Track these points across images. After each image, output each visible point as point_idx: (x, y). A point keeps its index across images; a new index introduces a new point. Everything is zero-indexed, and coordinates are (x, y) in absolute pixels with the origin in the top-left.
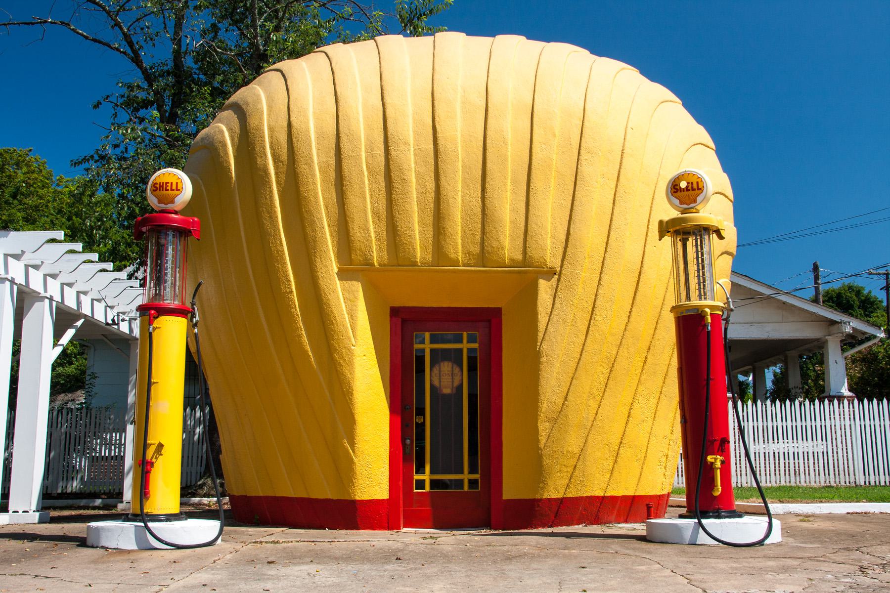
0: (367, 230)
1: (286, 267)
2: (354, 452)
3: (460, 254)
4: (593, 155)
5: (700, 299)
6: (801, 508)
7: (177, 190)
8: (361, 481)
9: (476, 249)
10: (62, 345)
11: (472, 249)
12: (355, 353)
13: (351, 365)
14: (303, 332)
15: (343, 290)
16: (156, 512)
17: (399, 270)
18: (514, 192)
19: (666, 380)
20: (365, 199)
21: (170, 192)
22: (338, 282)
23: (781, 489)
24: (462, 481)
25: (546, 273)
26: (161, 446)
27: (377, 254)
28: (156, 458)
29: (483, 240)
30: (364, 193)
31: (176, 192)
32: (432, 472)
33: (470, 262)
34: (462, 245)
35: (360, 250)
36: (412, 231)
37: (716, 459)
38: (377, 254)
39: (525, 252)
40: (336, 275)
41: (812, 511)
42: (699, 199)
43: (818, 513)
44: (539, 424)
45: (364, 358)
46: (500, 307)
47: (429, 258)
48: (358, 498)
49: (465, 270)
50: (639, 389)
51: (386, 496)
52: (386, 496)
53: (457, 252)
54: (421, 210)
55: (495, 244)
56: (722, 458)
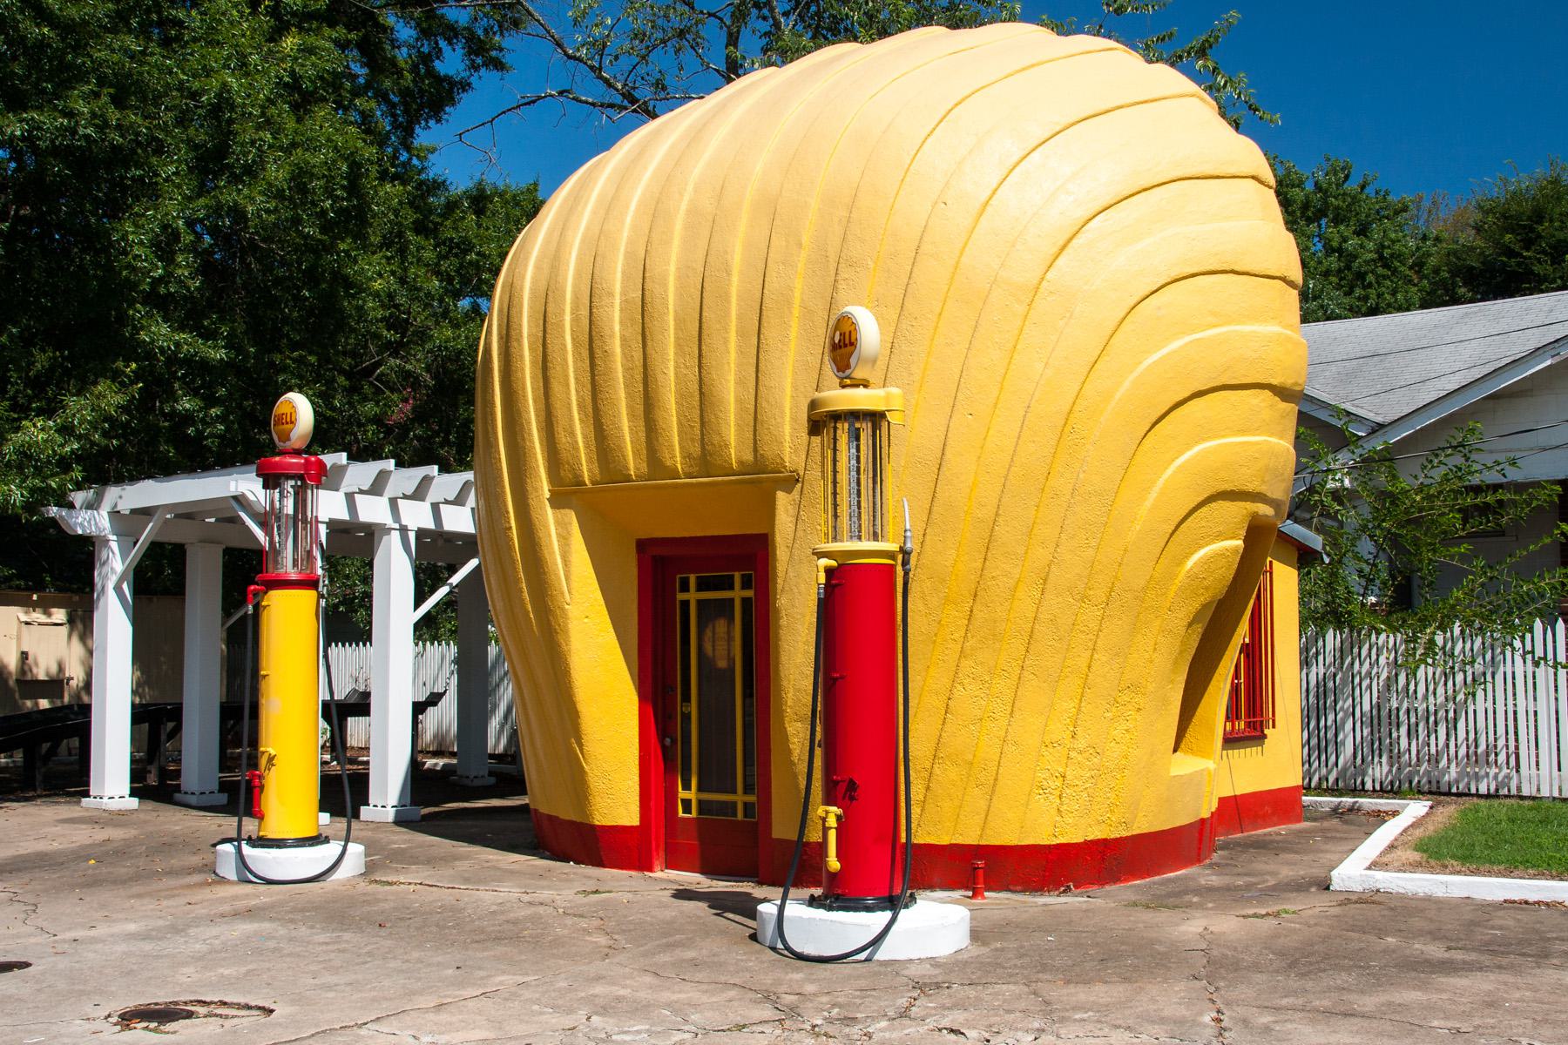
0: (572, 434)
1: (504, 493)
2: (582, 754)
3: (678, 459)
4: (858, 270)
5: (835, 539)
6: (1401, 883)
7: (292, 422)
8: (598, 799)
9: (696, 450)
10: (451, 584)
11: (692, 450)
12: (570, 615)
13: (566, 632)
14: (524, 585)
15: (557, 523)
16: (271, 836)
17: (616, 489)
18: (740, 352)
19: (1032, 647)
20: (568, 385)
21: (285, 426)
22: (549, 511)
23: (1396, 844)
24: (734, 804)
25: (786, 480)
26: (271, 759)
27: (587, 470)
28: (269, 770)
29: (702, 434)
30: (567, 376)
31: (290, 426)
32: (700, 789)
33: (691, 470)
34: (680, 444)
35: (568, 463)
36: (619, 429)
37: (827, 812)
38: (587, 470)
39: (755, 450)
40: (547, 503)
41: (1427, 891)
42: (853, 361)
43: (1440, 895)
44: (787, 725)
45: (586, 620)
46: (766, 532)
47: (644, 468)
48: (597, 823)
49: (687, 484)
50: (962, 665)
51: (634, 820)
52: (634, 820)
53: (674, 457)
54: (629, 395)
55: (716, 440)
56: (839, 811)
